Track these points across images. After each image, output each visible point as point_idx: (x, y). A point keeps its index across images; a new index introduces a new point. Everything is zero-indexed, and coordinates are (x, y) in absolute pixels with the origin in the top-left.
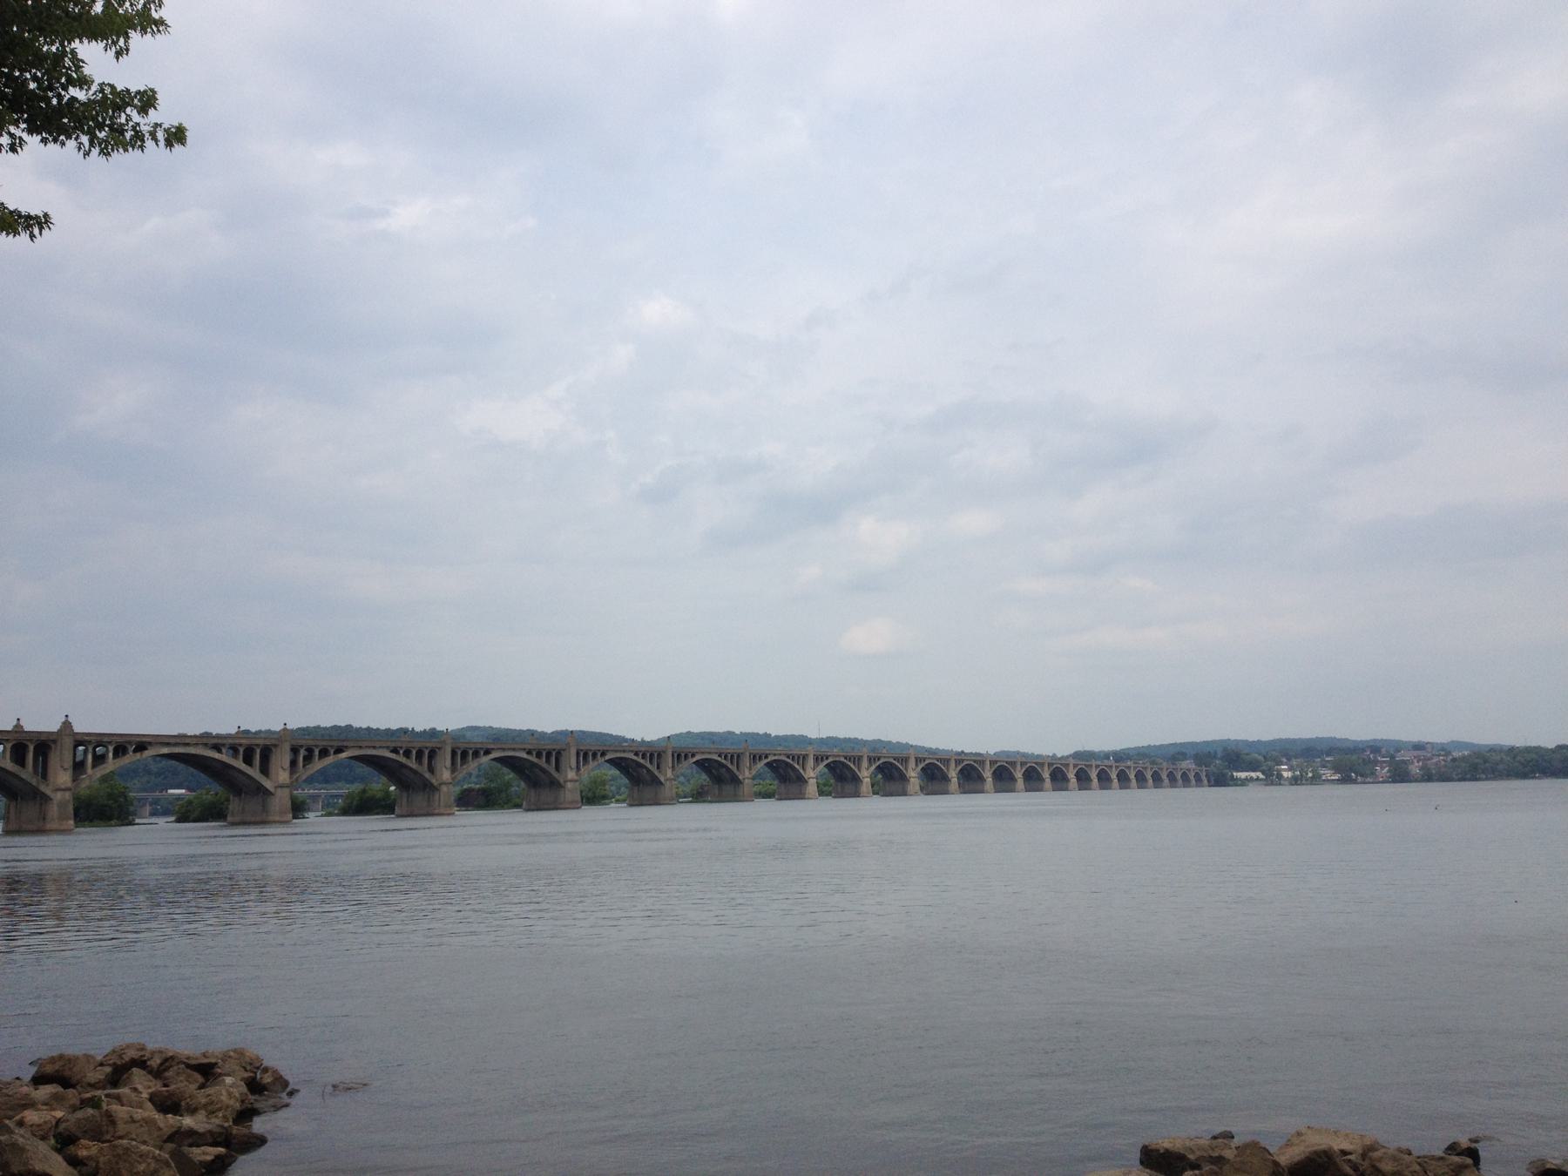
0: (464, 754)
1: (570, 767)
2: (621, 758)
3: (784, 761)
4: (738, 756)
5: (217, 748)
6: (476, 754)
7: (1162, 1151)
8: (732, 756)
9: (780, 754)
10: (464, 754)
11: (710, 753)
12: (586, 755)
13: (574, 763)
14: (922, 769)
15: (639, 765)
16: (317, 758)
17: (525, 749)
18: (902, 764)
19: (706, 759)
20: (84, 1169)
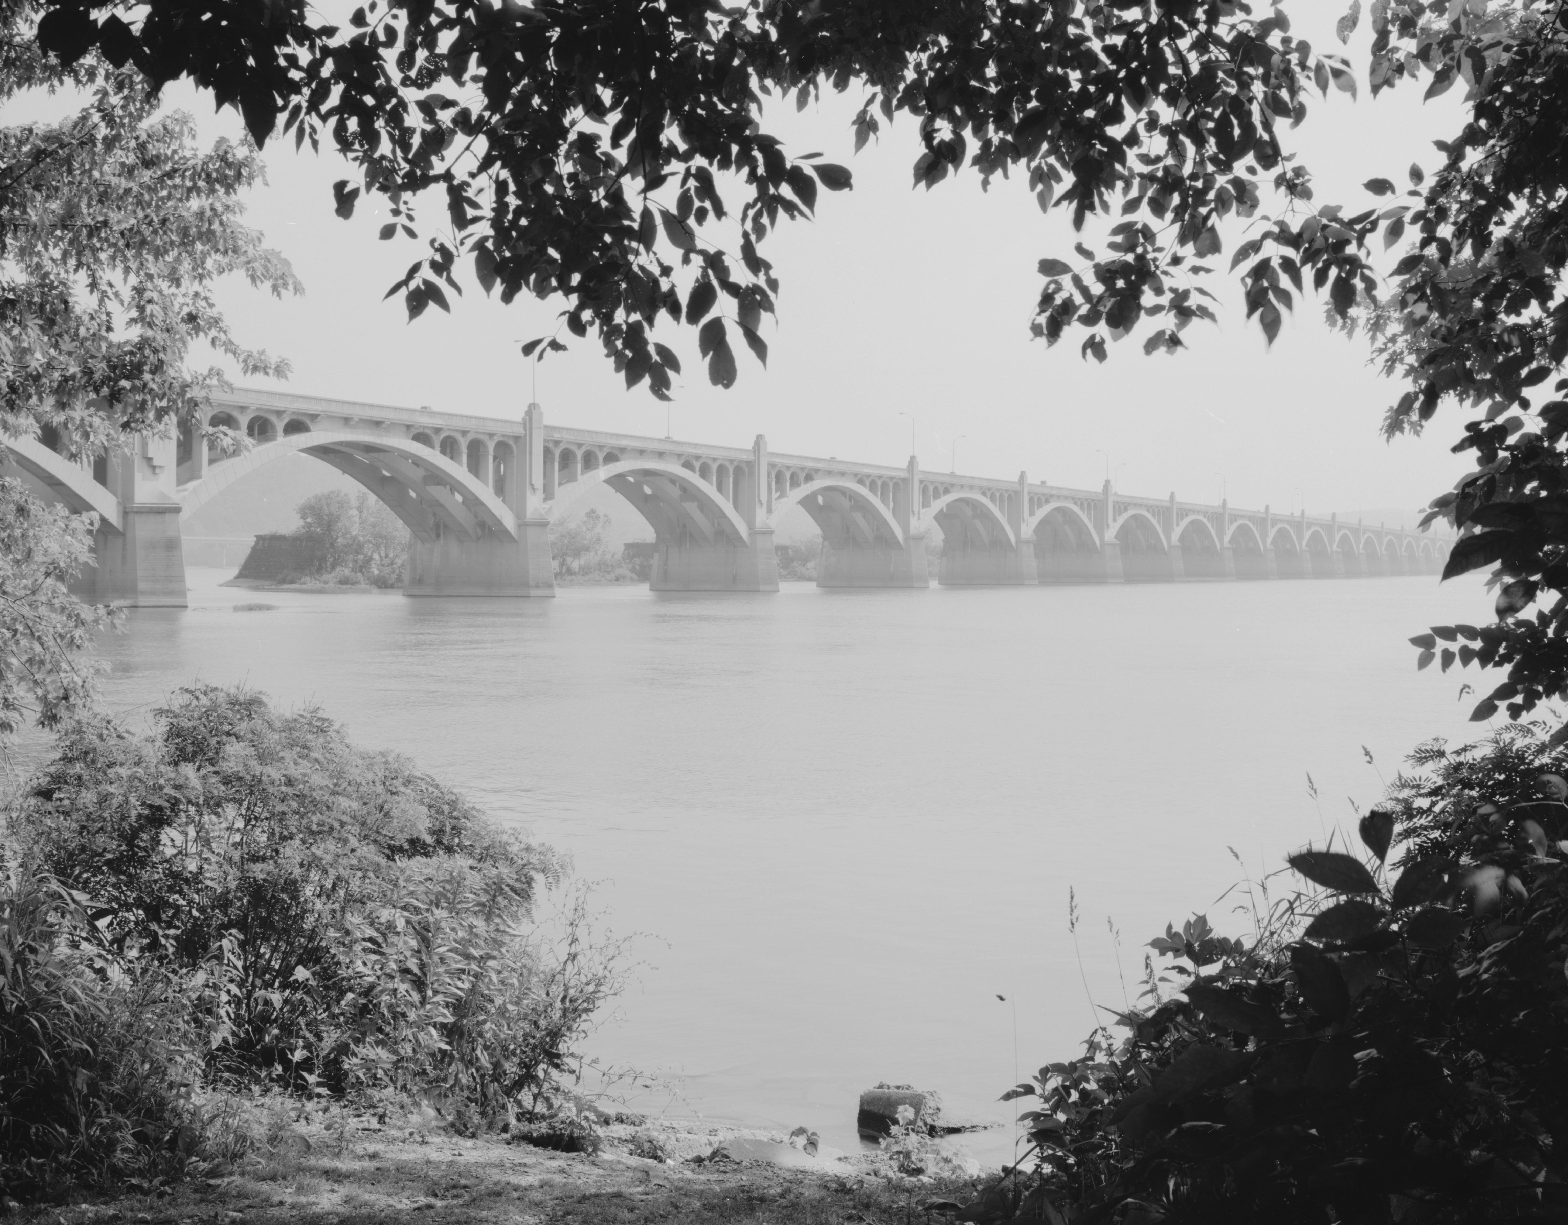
0: (567, 458)
1: (532, 485)
2: (369, 449)
3: (673, 480)
4: (738, 470)
5: (422, 437)
6: (589, 461)
7: (1502, 249)
8: (884, 485)
9: (843, 474)
10: (567, 458)
11: (661, 455)
12: (779, 477)
13: (538, 479)
14: (936, 518)
15: (436, 477)
16: (579, 467)
17: (679, 456)
18: (884, 500)
19: (647, 473)
20: (7, 991)
